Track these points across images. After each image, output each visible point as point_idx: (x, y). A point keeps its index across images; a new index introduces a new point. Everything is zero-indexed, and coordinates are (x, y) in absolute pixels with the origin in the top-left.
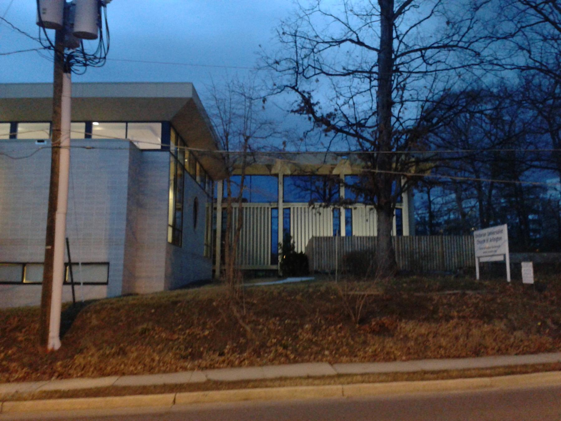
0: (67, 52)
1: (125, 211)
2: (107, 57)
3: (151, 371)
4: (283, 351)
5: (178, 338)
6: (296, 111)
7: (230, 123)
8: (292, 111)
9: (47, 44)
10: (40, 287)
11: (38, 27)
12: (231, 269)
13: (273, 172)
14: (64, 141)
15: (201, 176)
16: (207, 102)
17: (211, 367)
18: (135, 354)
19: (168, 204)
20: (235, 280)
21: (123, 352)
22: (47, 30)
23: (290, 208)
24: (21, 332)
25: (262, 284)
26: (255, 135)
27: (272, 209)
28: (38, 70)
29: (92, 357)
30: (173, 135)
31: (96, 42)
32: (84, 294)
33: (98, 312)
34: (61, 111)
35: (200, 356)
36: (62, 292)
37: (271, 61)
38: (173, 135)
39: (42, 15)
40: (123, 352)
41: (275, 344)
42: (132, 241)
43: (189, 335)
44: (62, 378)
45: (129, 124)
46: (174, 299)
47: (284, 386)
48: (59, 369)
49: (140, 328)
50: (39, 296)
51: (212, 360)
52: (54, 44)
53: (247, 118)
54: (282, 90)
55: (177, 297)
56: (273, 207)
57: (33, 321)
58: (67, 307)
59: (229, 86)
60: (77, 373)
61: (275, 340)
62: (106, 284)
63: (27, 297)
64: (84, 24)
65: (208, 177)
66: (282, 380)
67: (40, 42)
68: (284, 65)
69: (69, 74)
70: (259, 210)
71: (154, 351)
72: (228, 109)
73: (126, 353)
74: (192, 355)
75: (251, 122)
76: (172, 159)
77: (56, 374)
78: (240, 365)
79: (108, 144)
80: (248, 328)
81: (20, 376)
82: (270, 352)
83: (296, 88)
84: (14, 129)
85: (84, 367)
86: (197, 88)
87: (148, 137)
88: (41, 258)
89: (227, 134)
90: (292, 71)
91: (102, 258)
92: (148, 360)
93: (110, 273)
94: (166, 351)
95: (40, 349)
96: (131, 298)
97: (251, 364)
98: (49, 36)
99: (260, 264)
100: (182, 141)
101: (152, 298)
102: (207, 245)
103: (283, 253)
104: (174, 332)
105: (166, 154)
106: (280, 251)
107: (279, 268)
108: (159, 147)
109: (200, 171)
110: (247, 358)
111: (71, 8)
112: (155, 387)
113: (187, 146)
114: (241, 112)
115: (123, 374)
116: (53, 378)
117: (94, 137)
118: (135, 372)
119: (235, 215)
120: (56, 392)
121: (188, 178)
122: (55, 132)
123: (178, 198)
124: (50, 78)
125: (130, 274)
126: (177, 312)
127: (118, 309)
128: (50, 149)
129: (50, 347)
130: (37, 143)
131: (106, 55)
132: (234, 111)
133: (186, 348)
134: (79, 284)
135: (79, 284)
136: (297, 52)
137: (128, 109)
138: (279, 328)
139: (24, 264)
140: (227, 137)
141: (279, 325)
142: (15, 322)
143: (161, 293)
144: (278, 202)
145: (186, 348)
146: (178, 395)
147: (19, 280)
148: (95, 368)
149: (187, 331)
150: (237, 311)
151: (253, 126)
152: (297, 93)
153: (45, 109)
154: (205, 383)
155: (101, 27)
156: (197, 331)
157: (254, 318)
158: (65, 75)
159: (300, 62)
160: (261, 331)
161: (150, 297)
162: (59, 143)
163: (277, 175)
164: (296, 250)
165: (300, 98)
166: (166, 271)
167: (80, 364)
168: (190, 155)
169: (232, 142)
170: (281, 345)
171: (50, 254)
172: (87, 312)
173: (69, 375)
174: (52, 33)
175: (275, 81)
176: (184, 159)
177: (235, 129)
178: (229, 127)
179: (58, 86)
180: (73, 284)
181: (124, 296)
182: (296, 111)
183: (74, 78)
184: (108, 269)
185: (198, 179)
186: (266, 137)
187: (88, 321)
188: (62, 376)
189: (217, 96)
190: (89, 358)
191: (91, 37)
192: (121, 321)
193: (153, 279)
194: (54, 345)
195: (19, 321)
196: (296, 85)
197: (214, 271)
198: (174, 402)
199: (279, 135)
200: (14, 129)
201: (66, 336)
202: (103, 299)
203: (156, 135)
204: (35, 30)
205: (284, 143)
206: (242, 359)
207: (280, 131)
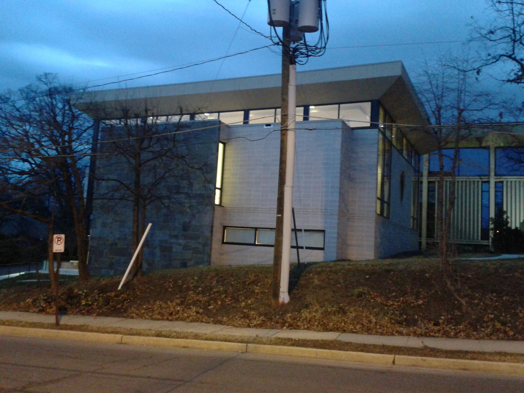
0: (293, 45)
1: (337, 185)
2: (327, 46)
3: (369, 331)
4: (502, 327)
5: (393, 305)
6: (514, 81)
7: (442, 97)
8: (509, 81)
9: (276, 40)
10: (272, 249)
11: (269, 26)
12: (444, 243)
13: (484, 145)
14: (291, 125)
15: (407, 150)
16: (416, 77)
17: (426, 335)
18: (354, 314)
19: (377, 179)
20: (448, 253)
21: (343, 311)
22: (276, 28)
23: (502, 182)
24: (257, 286)
25: (477, 259)
26: (470, 108)
27: (483, 182)
28: (271, 64)
29: (315, 312)
30: (381, 113)
31: (317, 34)
32: (307, 257)
33: (319, 273)
34: (288, 98)
35: (415, 323)
36: (291, 254)
37: (484, 32)
38: (381, 113)
39: (273, 16)
40: (343, 311)
41: (492, 320)
42: (345, 214)
43: (403, 302)
44: (291, 329)
45: (341, 105)
46: (387, 267)
47: (504, 361)
48: (289, 320)
49: (356, 291)
50: (272, 256)
51: (427, 329)
52: (282, 39)
53: (460, 91)
54: (497, 60)
55: (389, 265)
56: (484, 180)
57: (266, 277)
58: (293, 267)
59: (441, 62)
60: (304, 325)
61: (493, 316)
62: (322, 249)
63: (263, 257)
64: (306, 19)
65: (415, 152)
66: (503, 355)
67: (272, 40)
68: (499, 34)
69: (294, 65)
70: (464, 184)
71: (370, 314)
72: (440, 84)
73: (346, 313)
74: (406, 322)
75: (465, 95)
76: (381, 136)
77: (287, 325)
78: (456, 336)
79: (324, 125)
80: (463, 302)
81: (259, 322)
82: (488, 327)
83: (513, 56)
84: (246, 117)
85: (310, 321)
86: (404, 64)
87: (358, 116)
88: (274, 225)
89: (439, 108)
90: (509, 40)
91: (320, 227)
92: (365, 321)
93: (326, 240)
94: (382, 315)
95: (273, 301)
96: (346, 263)
97: (468, 337)
98: (278, 33)
99: (469, 238)
100: (390, 118)
101: (366, 265)
102: (414, 219)
103: (495, 229)
104: (388, 299)
105: (375, 131)
106: (492, 226)
107: (490, 244)
108: (368, 125)
109: (407, 146)
110: (463, 331)
111: (296, 6)
112: (375, 346)
113: (395, 123)
114: (453, 86)
115: (344, 331)
116: (285, 328)
117: (311, 119)
118: (355, 330)
119: (446, 190)
120: (289, 340)
121: (395, 153)
122: (285, 117)
123: (385, 174)
124: (278, 70)
125: (343, 242)
126: (390, 280)
127: (336, 273)
128: (280, 132)
129: (281, 300)
130: (265, 127)
131: (326, 44)
132: (447, 85)
133: (401, 315)
134: (302, 248)
135: (302, 248)
136: (513, 20)
137: (341, 92)
138: (497, 304)
139: (256, 229)
140: (439, 111)
141: (496, 301)
142: (252, 277)
143: (372, 260)
144: (489, 175)
145: (401, 315)
146: (397, 356)
147: (253, 243)
148: (319, 323)
149: (401, 299)
150: (452, 285)
151: (468, 100)
152: (514, 62)
153: (273, 97)
154: (422, 349)
155: (321, 20)
156: (411, 299)
157: (469, 292)
158: (291, 66)
159: (517, 29)
160: (478, 305)
161: (363, 264)
162: (287, 126)
163: (487, 148)
164: (509, 225)
165: (518, 67)
166: (375, 242)
167: (306, 318)
168: (397, 131)
169: (444, 116)
170: (499, 321)
171: (280, 221)
172: (309, 273)
173: (298, 326)
174: (280, 30)
175: (489, 52)
176: (392, 134)
177: (447, 103)
178: (442, 101)
179: (285, 76)
180: (298, 247)
181: (339, 260)
182: (514, 81)
183: (299, 68)
184: (324, 235)
185: (405, 152)
186: (482, 110)
187: (311, 280)
188: (293, 326)
189: (430, 72)
190: (314, 314)
191: (312, 29)
192: (339, 283)
193: (364, 248)
194: (284, 299)
195: (255, 276)
196: (513, 54)
197: (420, 243)
198: (394, 362)
199: (496, 106)
200: (246, 117)
201: (294, 292)
202: (321, 262)
203: (365, 112)
204: (267, 29)
205: (501, 115)
206: (458, 331)
207: (497, 102)
